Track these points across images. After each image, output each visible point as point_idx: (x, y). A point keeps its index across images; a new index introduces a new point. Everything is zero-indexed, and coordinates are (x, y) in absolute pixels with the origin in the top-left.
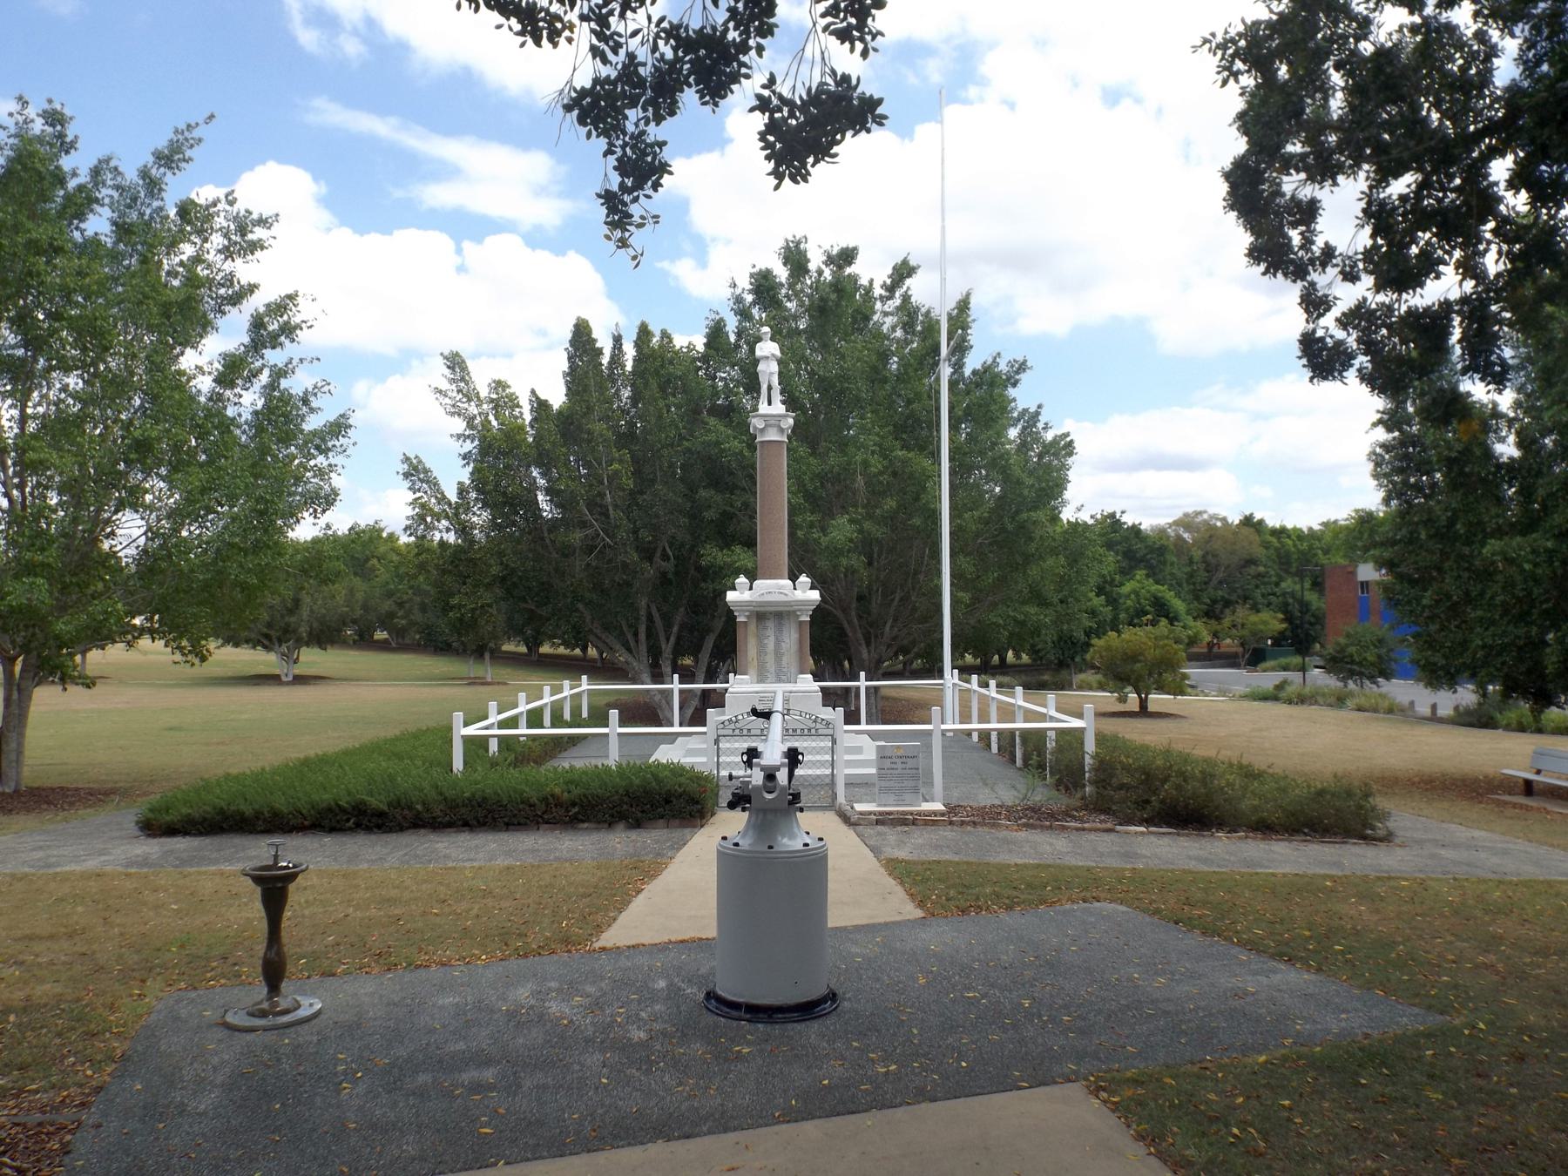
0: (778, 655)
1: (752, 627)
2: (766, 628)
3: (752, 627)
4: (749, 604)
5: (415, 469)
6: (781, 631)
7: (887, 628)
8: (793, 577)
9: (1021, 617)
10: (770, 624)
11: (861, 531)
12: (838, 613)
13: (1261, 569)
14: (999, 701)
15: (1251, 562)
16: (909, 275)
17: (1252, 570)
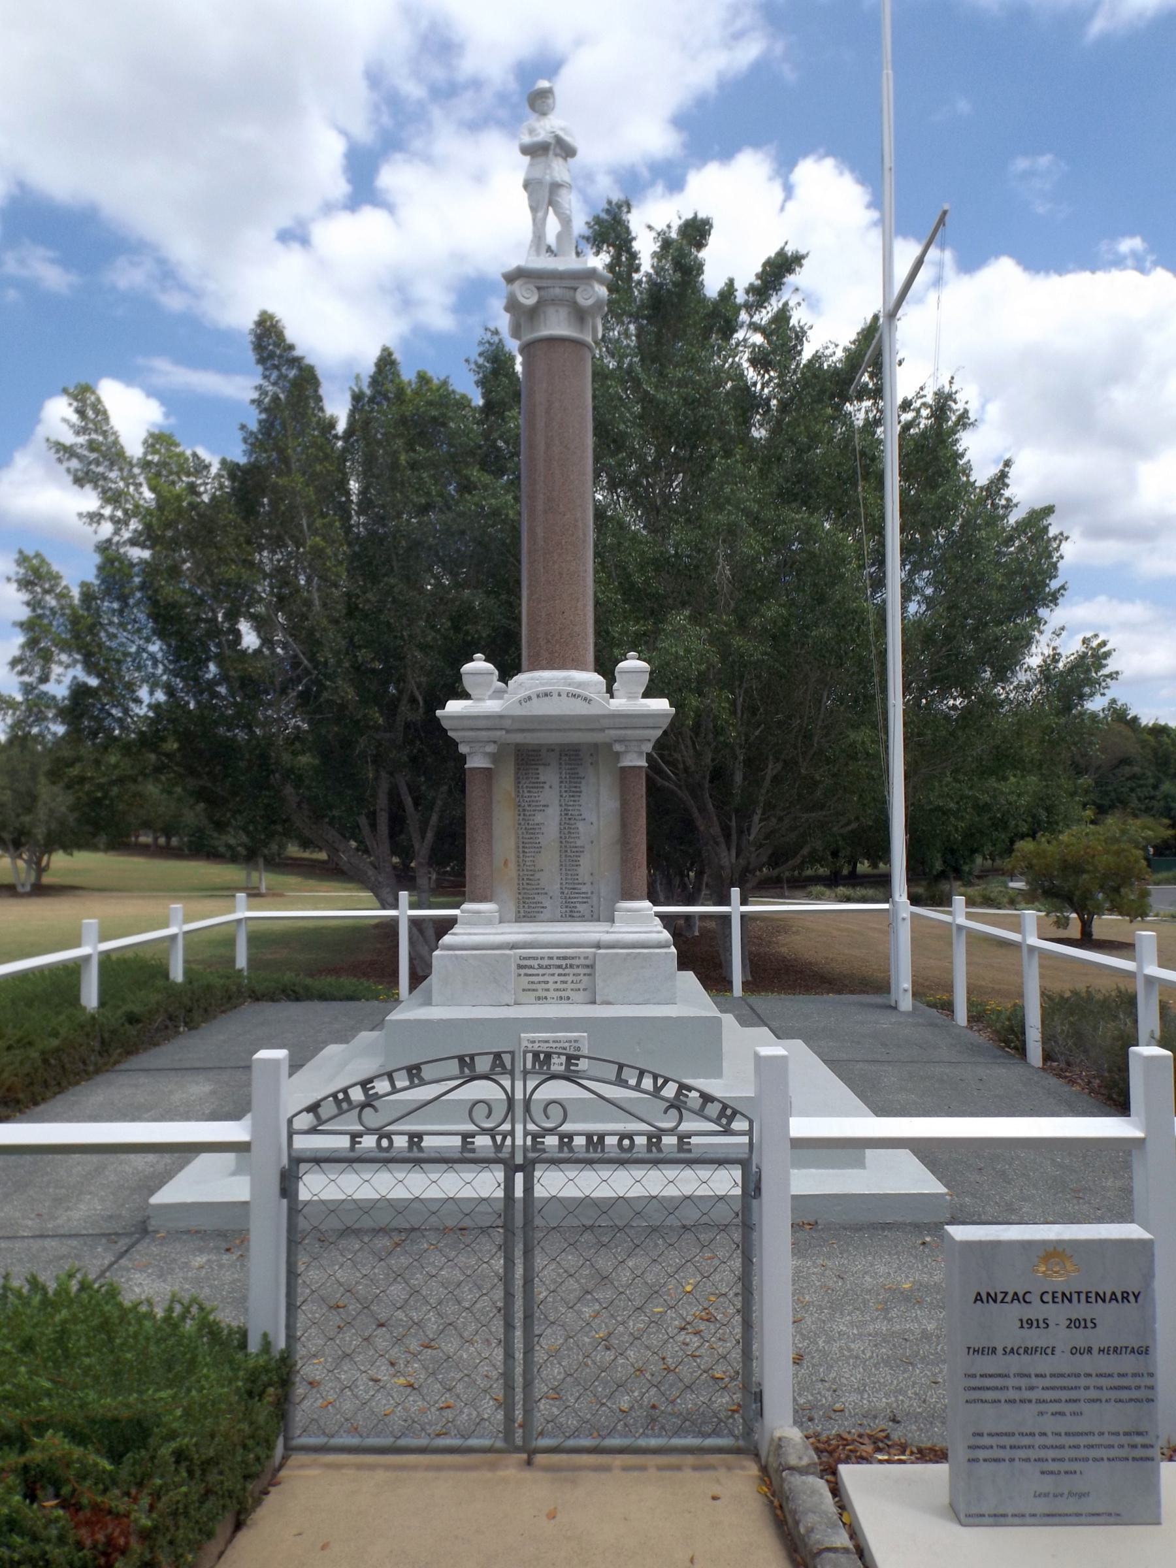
0: (569, 853)
1: (505, 784)
2: (539, 786)
3: (505, 784)
4: (493, 722)
5: (36, 571)
6: (576, 793)
7: (756, 818)
8: (606, 667)
9: (986, 798)
10: (550, 776)
11: (725, 654)
12: (684, 795)
13: (1136, 769)
14: (970, 932)
15: (1125, 761)
16: (790, 271)
17: (1127, 770)
